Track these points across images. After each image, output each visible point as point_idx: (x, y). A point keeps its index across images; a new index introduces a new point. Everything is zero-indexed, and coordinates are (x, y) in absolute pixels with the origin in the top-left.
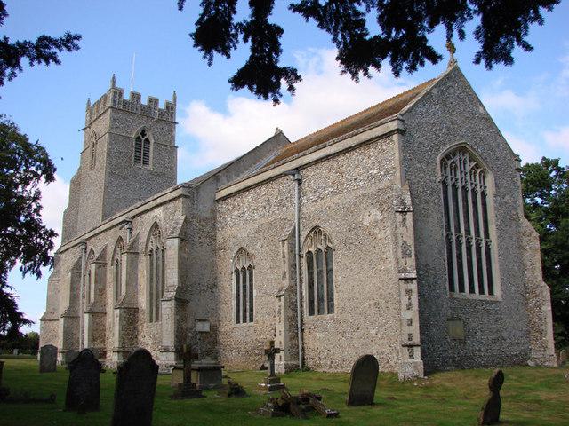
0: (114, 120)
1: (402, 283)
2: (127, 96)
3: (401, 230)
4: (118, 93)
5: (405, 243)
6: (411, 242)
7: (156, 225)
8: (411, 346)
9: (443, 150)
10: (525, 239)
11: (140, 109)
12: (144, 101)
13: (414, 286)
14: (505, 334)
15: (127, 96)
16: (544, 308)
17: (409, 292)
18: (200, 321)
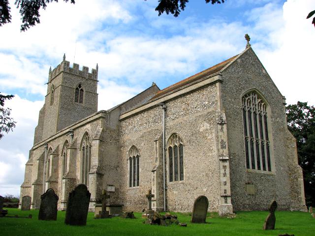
0: (64, 78)
1: (221, 162)
2: (71, 66)
5: (222, 141)
6: (225, 140)
7: (86, 134)
8: (226, 197)
9: (243, 92)
12: (81, 69)
14: (277, 193)
15: (71, 66)
16: (299, 179)
18: (110, 185)
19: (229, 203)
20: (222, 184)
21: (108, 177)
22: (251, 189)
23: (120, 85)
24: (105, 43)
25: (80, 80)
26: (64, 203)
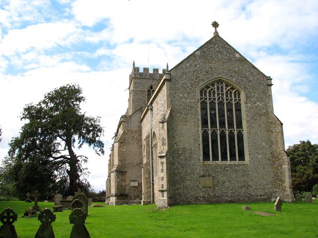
0: (135, 83)
1: (159, 159)
2: (141, 71)
3: (162, 131)
4: (136, 70)
5: (163, 138)
6: (166, 137)
8: (162, 191)
9: (202, 85)
10: (273, 126)
11: (149, 76)
12: (151, 72)
13: (164, 160)
14: (251, 183)
15: (141, 71)
16: (283, 166)
17: (162, 163)
18: (132, 181)
19: (165, 198)
20: (160, 180)
21: (130, 175)
22: (208, 182)
23: (271, 54)
24: (244, 9)
25: (150, 82)
26: (115, 196)
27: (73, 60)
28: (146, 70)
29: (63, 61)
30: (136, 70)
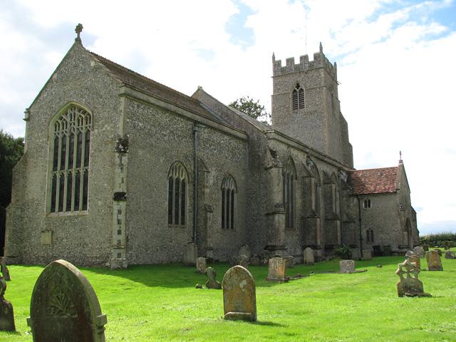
2: (284, 64)
4: (277, 64)
12: (297, 62)
15: (284, 64)
27: (411, 19)
28: (304, 58)
29: (395, 25)
30: (277, 64)
